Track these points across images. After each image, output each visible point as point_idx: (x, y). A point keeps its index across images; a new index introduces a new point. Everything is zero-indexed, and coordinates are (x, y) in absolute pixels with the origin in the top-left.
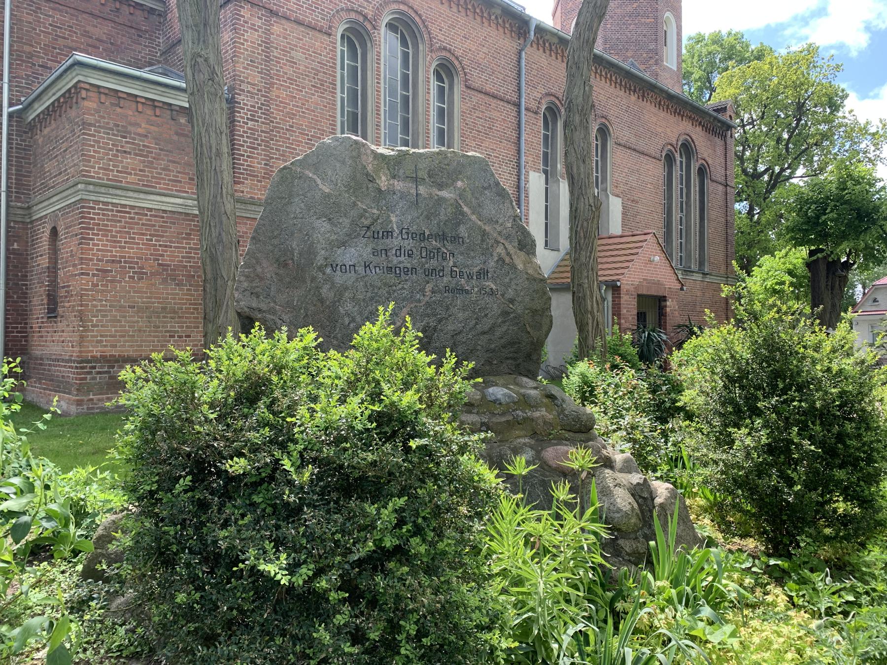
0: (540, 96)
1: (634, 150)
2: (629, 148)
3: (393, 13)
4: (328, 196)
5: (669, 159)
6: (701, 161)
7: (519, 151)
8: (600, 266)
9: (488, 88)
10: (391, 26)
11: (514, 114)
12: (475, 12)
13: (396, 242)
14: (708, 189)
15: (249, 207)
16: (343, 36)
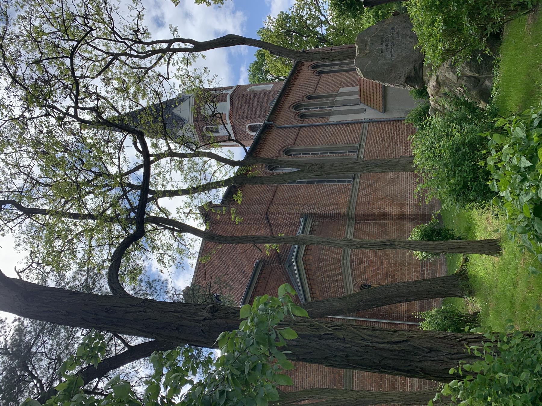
4: (372, 62)
5: (320, 73)
7: (320, 125)
8: (348, 237)
11: (304, 128)
13: (384, 47)
15: (351, 208)
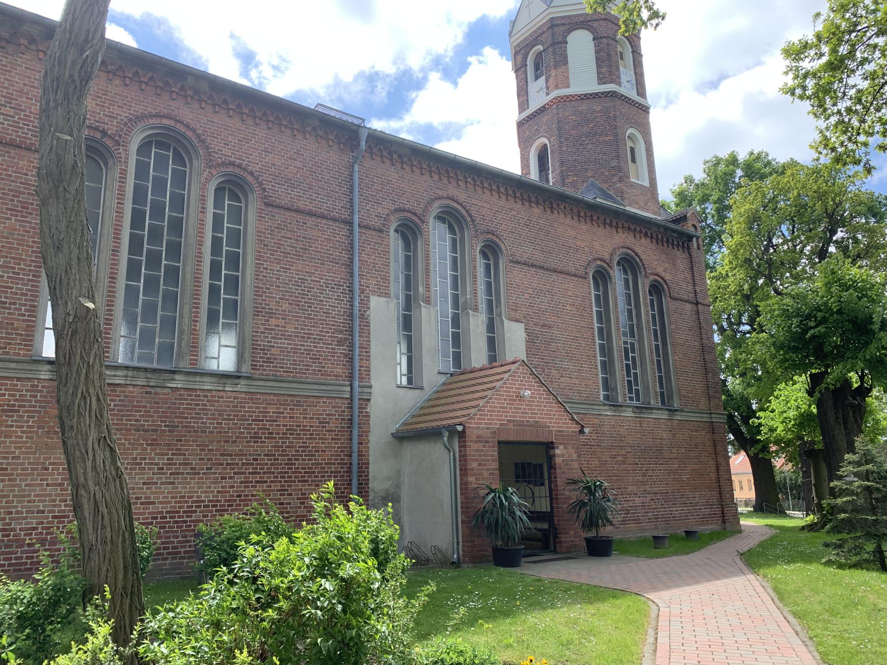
0: (387, 212)
1: (542, 268)
2: (533, 266)
3: (152, 128)
5: (602, 278)
6: (652, 277)
9: (301, 205)
10: (440, 218)
12: (412, 165)
14: (668, 308)
16: (396, 231)
